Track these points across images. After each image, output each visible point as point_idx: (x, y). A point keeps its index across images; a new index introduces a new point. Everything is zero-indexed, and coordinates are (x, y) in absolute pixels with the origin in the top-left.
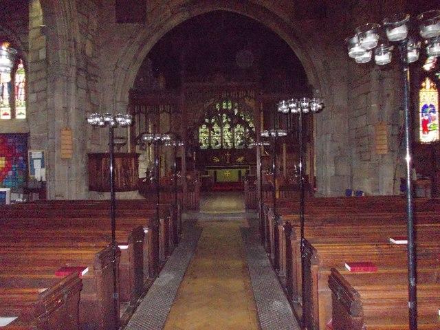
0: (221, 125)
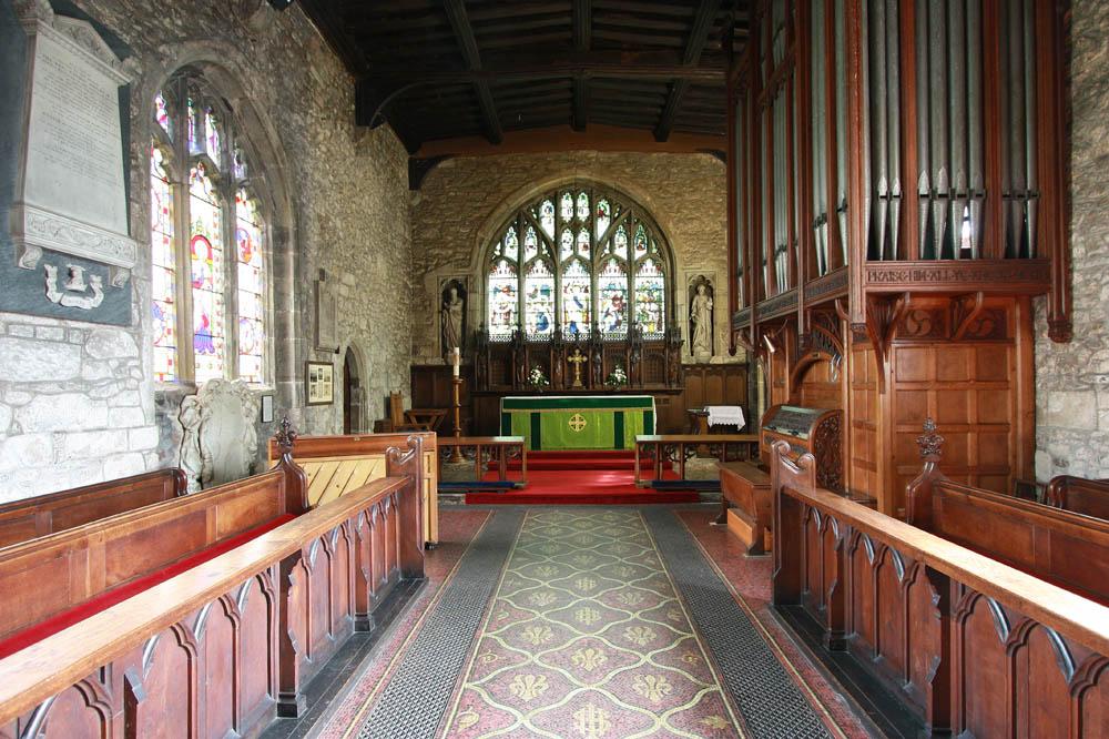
0: (554, 266)
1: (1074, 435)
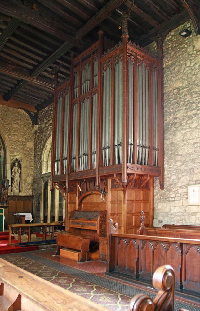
1: (164, 214)
